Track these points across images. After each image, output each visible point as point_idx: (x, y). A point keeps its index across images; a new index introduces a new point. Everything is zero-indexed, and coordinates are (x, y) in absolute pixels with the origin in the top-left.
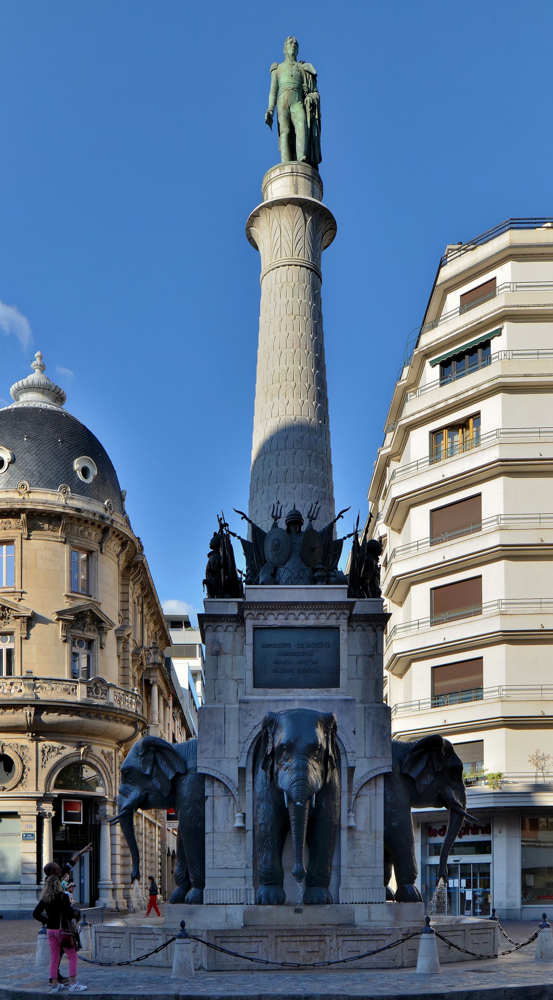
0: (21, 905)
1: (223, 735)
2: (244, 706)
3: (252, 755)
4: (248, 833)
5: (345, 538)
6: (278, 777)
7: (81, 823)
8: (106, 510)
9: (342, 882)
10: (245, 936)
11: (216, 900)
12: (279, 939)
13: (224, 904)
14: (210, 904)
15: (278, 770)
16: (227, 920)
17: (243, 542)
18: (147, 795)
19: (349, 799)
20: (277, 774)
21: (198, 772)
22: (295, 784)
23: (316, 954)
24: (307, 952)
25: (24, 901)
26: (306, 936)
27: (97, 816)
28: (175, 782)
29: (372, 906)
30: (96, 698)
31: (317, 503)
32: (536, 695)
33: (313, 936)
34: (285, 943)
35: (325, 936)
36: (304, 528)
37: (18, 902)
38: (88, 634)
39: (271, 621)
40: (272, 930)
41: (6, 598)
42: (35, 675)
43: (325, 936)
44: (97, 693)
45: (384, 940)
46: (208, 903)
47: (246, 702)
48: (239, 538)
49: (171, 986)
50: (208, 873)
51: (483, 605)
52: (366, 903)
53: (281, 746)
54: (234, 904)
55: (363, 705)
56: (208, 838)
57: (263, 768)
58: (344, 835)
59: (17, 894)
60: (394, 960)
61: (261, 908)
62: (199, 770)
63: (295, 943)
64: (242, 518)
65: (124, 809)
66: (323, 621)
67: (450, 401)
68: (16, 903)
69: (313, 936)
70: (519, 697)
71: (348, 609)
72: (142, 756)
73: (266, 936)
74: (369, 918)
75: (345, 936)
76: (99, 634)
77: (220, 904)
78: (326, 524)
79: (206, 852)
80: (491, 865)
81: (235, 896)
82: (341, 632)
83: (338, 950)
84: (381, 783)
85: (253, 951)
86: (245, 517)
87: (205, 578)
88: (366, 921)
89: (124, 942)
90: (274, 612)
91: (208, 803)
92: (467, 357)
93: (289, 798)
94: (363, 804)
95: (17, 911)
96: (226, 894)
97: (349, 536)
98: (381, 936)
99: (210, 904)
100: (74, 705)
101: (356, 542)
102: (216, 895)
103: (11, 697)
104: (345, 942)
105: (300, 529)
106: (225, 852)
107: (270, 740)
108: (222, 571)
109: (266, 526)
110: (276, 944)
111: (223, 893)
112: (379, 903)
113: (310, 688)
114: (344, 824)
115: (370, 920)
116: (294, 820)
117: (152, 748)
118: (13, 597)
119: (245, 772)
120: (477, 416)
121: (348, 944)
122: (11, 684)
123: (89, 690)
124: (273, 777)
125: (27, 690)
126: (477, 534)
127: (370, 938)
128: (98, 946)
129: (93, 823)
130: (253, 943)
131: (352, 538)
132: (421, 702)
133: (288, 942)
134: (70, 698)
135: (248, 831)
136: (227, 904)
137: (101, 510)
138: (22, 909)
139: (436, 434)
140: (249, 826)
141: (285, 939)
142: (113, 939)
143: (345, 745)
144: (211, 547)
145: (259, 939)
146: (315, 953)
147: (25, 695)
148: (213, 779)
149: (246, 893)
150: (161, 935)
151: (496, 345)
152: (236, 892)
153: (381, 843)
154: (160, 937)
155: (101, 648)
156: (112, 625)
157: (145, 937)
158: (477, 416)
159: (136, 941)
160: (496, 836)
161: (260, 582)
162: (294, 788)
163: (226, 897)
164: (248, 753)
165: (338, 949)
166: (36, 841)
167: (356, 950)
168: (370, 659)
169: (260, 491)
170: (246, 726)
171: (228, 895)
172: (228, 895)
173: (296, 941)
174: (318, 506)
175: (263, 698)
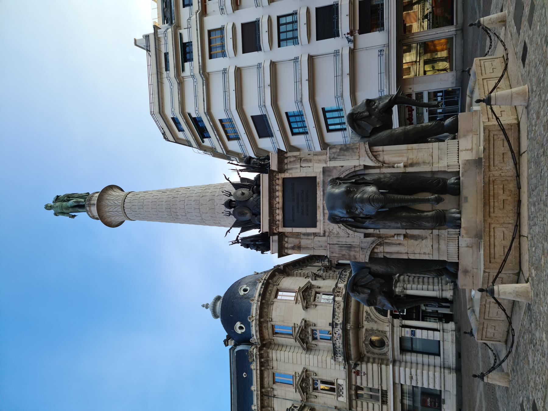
0: (452, 342)
1: (345, 245)
3: (356, 229)
4: (408, 232)
5: (240, 177)
6: (368, 215)
7: (405, 314)
8: (260, 282)
9: (443, 169)
10: (489, 240)
11: (456, 253)
12: (492, 215)
13: (458, 249)
14: (458, 257)
15: (363, 214)
16: (470, 246)
17: (242, 231)
18: (384, 292)
19: (386, 167)
20: (366, 215)
21: (368, 262)
22: (372, 204)
23: (505, 187)
24: (503, 193)
25: (450, 339)
26: (489, 195)
27: (402, 296)
28: (375, 275)
29: (461, 148)
30: (342, 293)
31: (223, 192)
32: (339, 79)
33: (489, 189)
34: (495, 210)
35: (489, 180)
37: (450, 343)
38: (313, 294)
39: (279, 217)
40: (484, 221)
41: (297, 331)
42: (331, 322)
43: (489, 180)
44: (340, 292)
45: (494, 135)
46: (457, 259)
48: (239, 234)
49: (544, 312)
50: (436, 258)
52: (458, 153)
53: (347, 212)
54: (458, 242)
55: (328, 162)
56: (412, 257)
57: (364, 223)
58: (410, 170)
59: (445, 343)
61: (463, 225)
62: (367, 261)
63: (496, 202)
64: (229, 232)
65: (393, 307)
66: (279, 188)
67: (216, 133)
68: (451, 345)
69: (489, 189)
71: (273, 173)
72: (359, 293)
73: (489, 225)
74: (470, 150)
75: (489, 165)
76: (313, 288)
77: (458, 251)
78: (232, 186)
79: (421, 258)
80: (429, 91)
81: (452, 241)
82: (286, 177)
83: (502, 170)
84: (376, 148)
85: (503, 234)
86: (229, 231)
87: (260, 252)
88: (472, 152)
89: (491, 323)
90: (275, 216)
91: (388, 256)
92: (228, 134)
93: (382, 207)
94: (387, 158)
96: (451, 246)
97: (239, 174)
98: (490, 138)
99: (458, 257)
101: (241, 170)
102: (452, 253)
103: (342, 334)
104: (495, 165)
105: (234, 201)
106: (421, 246)
107: (345, 219)
108: (257, 243)
109: (233, 220)
110: (496, 217)
111: (450, 249)
112: (458, 144)
113: (317, 194)
114: (401, 170)
115: (471, 150)
116: (398, 204)
117: (355, 288)
118: (297, 328)
119: (367, 234)
120: (221, 121)
122: (335, 334)
123: (338, 296)
124: (368, 217)
125: (338, 326)
126: (267, 116)
127: (491, 146)
128: (493, 339)
129: (405, 298)
130: (496, 235)
131: (240, 172)
132: (343, 136)
133: (495, 208)
135: (406, 233)
136: (458, 246)
137: (261, 284)
138: (454, 341)
139: (229, 139)
140: (403, 232)
141: (492, 210)
142: (488, 330)
143: (350, 172)
144: (248, 248)
145: (492, 230)
146: (504, 187)
148: (372, 252)
149: (451, 234)
150: (486, 300)
151: (194, 115)
152: (449, 240)
153: (415, 146)
154: (488, 300)
155: (320, 288)
156: (309, 282)
157: (487, 310)
158: (221, 121)
159: (491, 315)
160: (413, 90)
161: (260, 223)
162: (375, 204)
163: (453, 249)
164: (355, 231)
165: (501, 169)
166: (415, 330)
167: (502, 156)
168: (302, 159)
169: (220, 221)
170: (338, 233)
171: (452, 245)
172: (452, 245)
173: (494, 202)
174: (224, 192)
175: (322, 222)
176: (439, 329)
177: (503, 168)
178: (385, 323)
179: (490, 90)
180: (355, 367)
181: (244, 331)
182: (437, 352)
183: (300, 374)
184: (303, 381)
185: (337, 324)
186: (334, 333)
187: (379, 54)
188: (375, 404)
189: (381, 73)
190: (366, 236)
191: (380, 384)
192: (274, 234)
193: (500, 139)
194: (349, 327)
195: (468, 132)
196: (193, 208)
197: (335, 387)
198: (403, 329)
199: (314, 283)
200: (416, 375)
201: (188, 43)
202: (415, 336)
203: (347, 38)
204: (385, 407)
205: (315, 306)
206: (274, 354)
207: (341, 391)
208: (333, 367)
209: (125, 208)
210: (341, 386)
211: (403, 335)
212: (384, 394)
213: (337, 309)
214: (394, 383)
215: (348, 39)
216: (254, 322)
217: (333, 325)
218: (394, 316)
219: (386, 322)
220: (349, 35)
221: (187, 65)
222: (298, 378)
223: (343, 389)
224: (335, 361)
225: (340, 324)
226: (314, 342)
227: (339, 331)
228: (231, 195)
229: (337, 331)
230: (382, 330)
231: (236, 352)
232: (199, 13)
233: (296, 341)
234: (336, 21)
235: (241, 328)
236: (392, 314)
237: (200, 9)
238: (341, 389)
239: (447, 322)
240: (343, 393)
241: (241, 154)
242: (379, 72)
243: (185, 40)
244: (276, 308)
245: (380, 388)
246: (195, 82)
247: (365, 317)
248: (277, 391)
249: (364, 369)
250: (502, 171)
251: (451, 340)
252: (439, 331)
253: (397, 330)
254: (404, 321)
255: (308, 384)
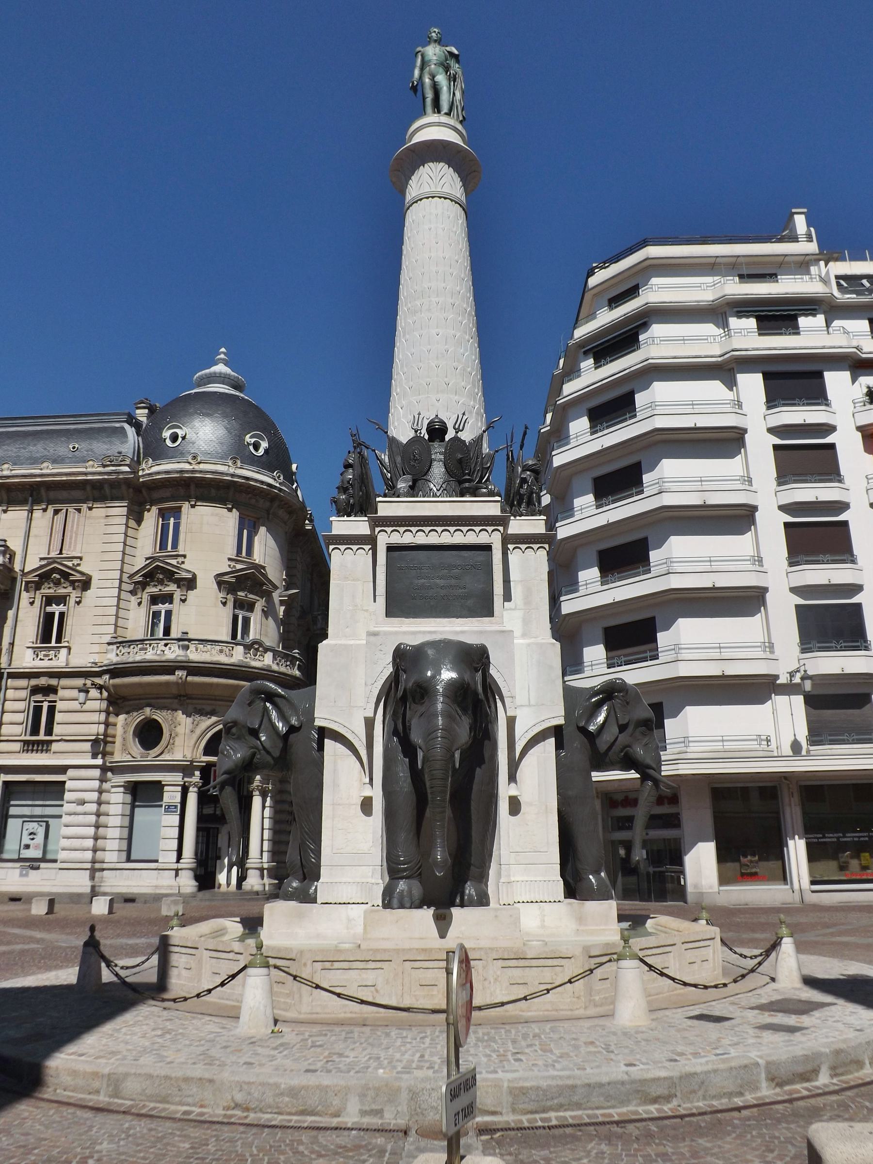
2: (372, 638)
36: (447, 438)
37: (155, 882)
42: (190, 636)
47: (375, 634)
51: (651, 564)
60: (578, 998)
68: (151, 885)
70: (696, 656)
82: (494, 551)
83: (494, 982)
84: (552, 741)
95: (151, 894)
100: (232, 667)
121: (510, 972)
122: (166, 645)
129: (245, 793)
134: (223, 659)
138: (158, 891)
145: (379, 965)
147: (178, 656)
150: (242, 954)
156: (276, 587)
166: (178, 813)
176: (181, 861)
177: (498, 983)
178: (191, 750)
179: (646, 959)
180: (96, 685)
181: (169, 443)
182: (133, 857)
183: (78, 568)
184: (65, 575)
185: (186, 648)
186: (166, 642)
187: (763, 737)
188: (21, 726)
189: (723, 741)
190: (369, 723)
191: (64, 738)
192: (372, 529)
193: (554, 977)
194: (179, 673)
195: (581, 919)
196: (429, 347)
197: (53, 644)
198: (179, 788)
199: (309, 1154)
200: (85, 814)
201: (797, 328)
202: (165, 811)
203: (798, 671)
204: (17, 746)
205: (224, 600)
206: (119, 510)
207: (45, 656)
208: (96, 639)
209: (430, 199)
210: (55, 656)
211: (166, 788)
212: (44, 746)
213: (218, 648)
214: (63, 769)
215: (796, 672)
216: (187, 467)
217: (185, 641)
218: (206, 771)
219: (195, 753)
220: (803, 673)
221: (752, 323)
222: (70, 564)
223: (49, 660)
224: (109, 644)
225: (187, 656)
226: (146, 597)
227: (173, 653)
228: (457, 432)
229: (170, 649)
230: (176, 744)
231: (123, 428)
232: (855, 352)
233: (147, 559)
234: (832, 647)
235: (256, 446)
236: (209, 766)
237: (864, 356)
238: (48, 656)
239: (197, 878)
240: (41, 659)
241: (560, 437)
242: (725, 738)
243: (803, 321)
244: (217, 515)
245: (53, 738)
246: (714, 339)
247: (203, 709)
248: (43, 517)
249: (90, 705)
250: (492, 981)
251: (161, 884)
252: (178, 861)
253: (177, 778)
254: (196, 789)
255: (57, 583)
